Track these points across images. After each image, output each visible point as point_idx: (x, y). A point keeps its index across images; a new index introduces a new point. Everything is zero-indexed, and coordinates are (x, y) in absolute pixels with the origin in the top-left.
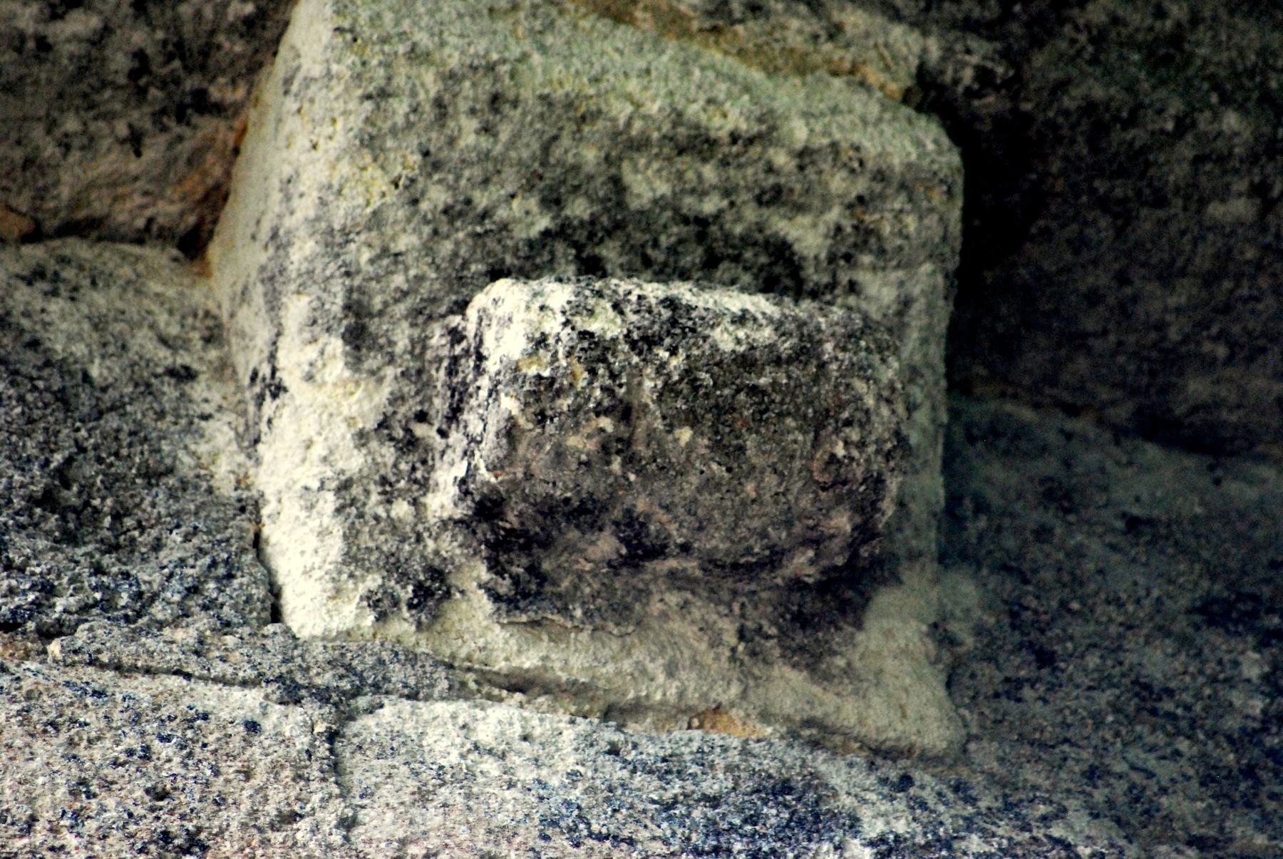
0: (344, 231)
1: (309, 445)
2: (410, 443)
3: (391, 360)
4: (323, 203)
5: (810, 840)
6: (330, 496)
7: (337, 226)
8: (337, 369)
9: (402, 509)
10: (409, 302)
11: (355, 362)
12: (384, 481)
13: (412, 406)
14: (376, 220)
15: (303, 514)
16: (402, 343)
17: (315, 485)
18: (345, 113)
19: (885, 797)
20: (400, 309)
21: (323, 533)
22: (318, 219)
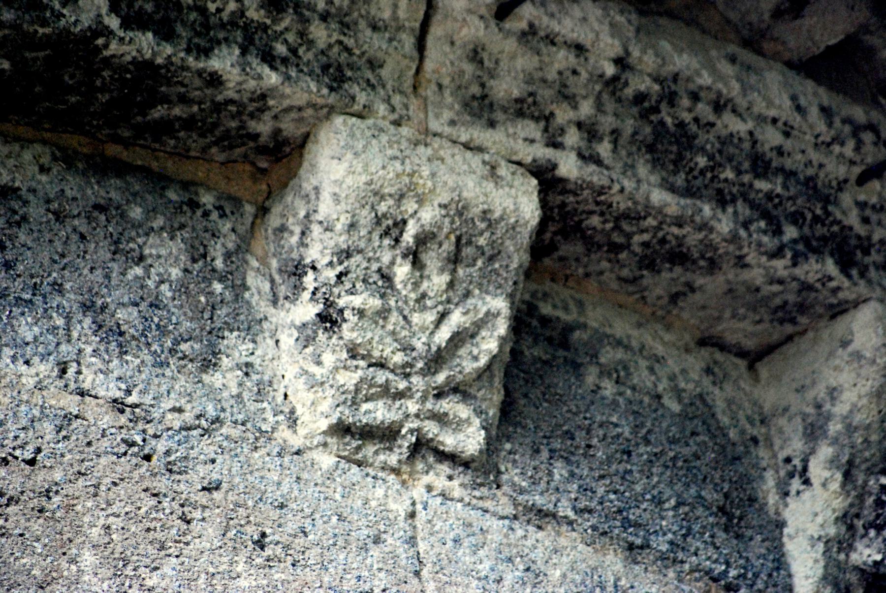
0: (856, 428)
1: (816, 515)
2: (851, 528)
3: (855, 488)
4: (851, 411)
5: (745, 490)
6: (822, 545)
7: (854, 424)
8: (835, 486)
9: (842, 557)
10: (869, 464)
11: (843, 485)
12: (840, 542)
13: (854, 511)
14: (868, 427)
15: (809, 548)
16: (860, 482)
17: (816, 536)
18: (874, 379)
19: (178, 209)
20: (864, 467)
21: (816, 561)
22: (846, 417)
